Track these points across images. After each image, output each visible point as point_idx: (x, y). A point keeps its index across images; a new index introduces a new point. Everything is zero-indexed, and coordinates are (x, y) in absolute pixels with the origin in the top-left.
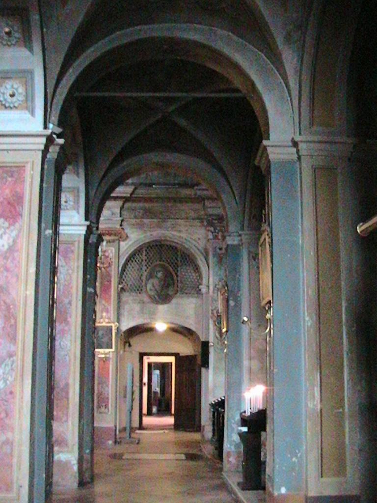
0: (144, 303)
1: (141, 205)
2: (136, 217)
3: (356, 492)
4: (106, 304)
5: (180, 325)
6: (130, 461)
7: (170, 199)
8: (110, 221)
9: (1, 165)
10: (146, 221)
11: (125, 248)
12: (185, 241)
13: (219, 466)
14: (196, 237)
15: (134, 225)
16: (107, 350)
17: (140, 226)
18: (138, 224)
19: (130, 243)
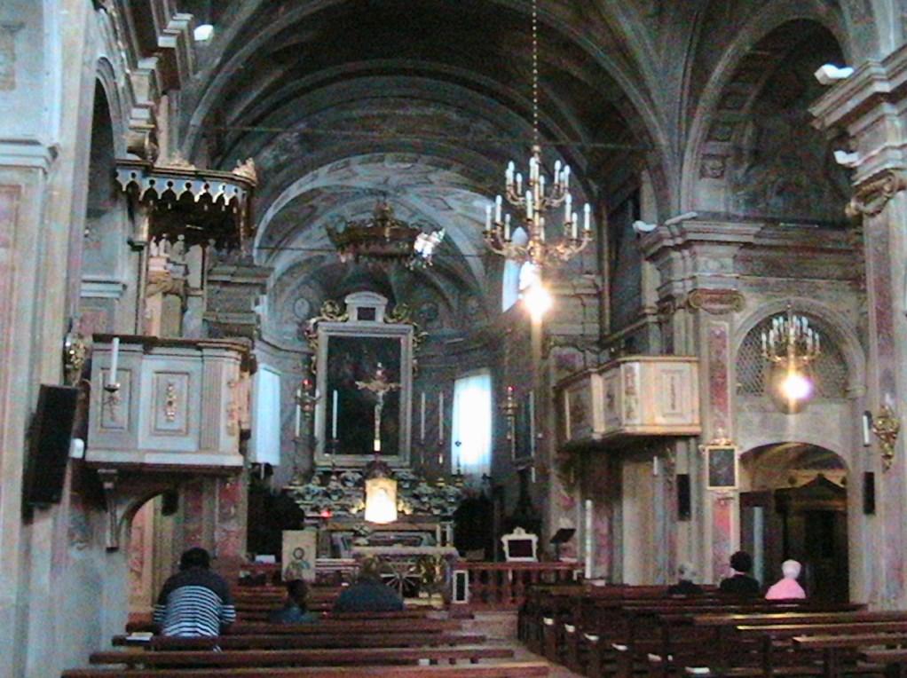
0: (765, 411)
1: (763, 253)
2: (753, 273)
3: (851, 600)
4: (721, 414)
5: (712, 393)
6: (43, 249)
7: (804, 248)
8: (718, 279)
9: (146, 4)
10: (772, 280)
11: (741, 323)
12: (828, 314)
13: (544, 486)
14: (844, 307)
15: (751, 285)
16: (726, 489)
17: (762, 288)
18: (758, 285)
19: (748, 315)
